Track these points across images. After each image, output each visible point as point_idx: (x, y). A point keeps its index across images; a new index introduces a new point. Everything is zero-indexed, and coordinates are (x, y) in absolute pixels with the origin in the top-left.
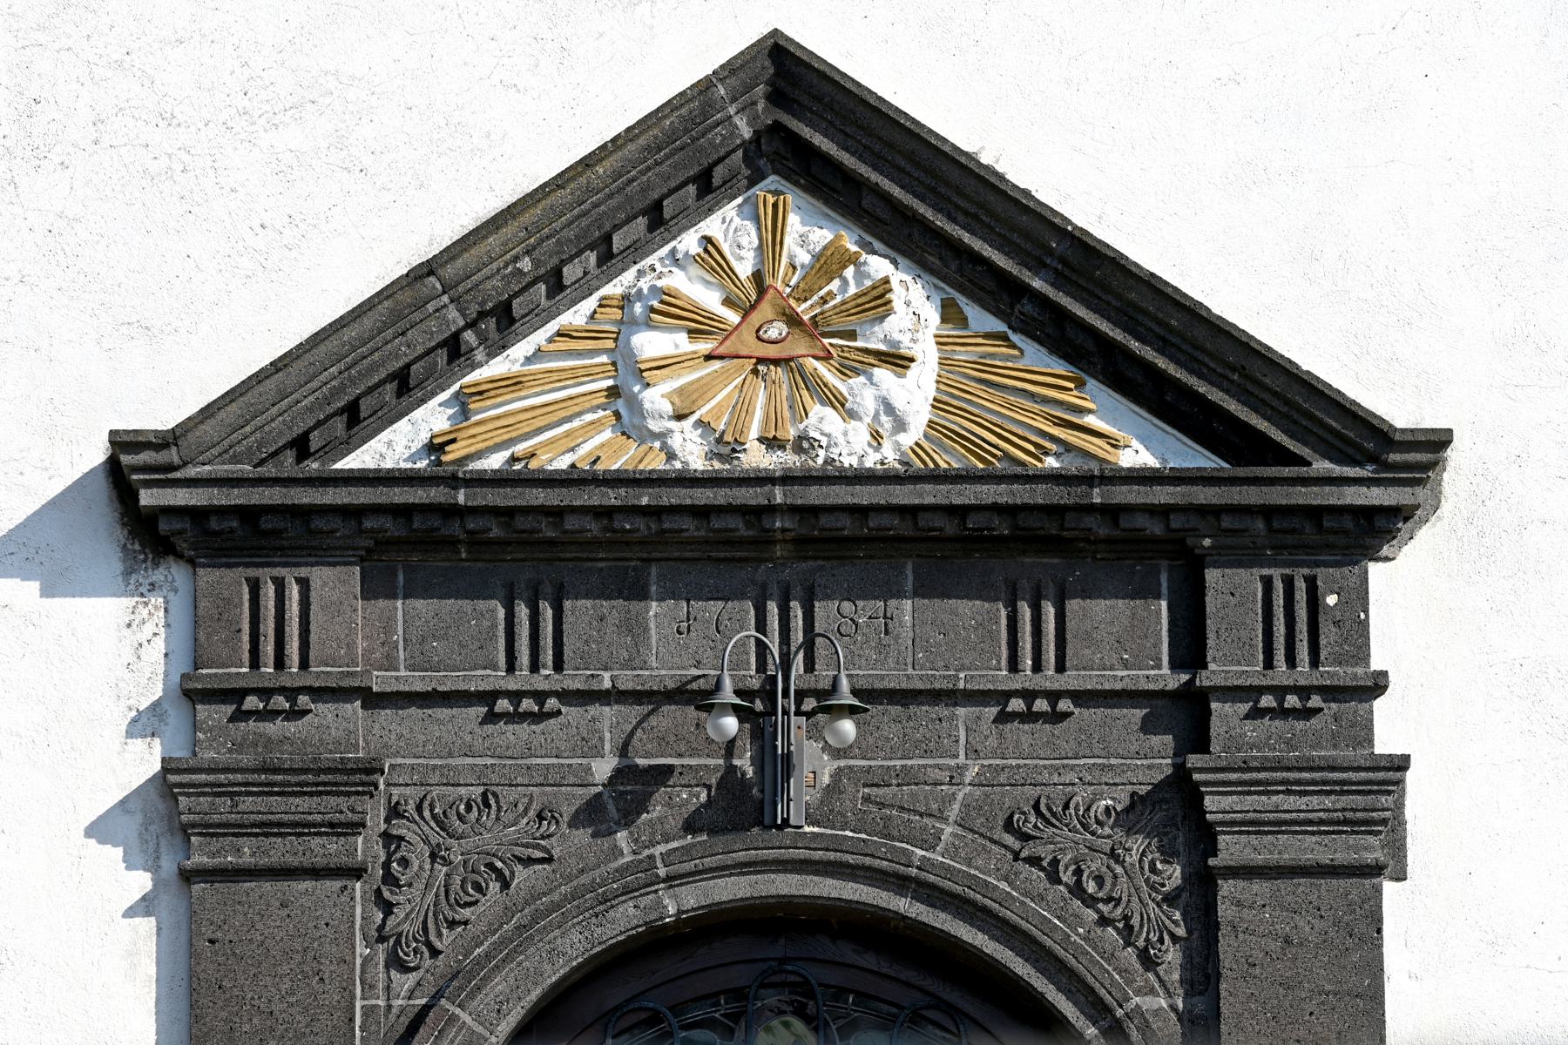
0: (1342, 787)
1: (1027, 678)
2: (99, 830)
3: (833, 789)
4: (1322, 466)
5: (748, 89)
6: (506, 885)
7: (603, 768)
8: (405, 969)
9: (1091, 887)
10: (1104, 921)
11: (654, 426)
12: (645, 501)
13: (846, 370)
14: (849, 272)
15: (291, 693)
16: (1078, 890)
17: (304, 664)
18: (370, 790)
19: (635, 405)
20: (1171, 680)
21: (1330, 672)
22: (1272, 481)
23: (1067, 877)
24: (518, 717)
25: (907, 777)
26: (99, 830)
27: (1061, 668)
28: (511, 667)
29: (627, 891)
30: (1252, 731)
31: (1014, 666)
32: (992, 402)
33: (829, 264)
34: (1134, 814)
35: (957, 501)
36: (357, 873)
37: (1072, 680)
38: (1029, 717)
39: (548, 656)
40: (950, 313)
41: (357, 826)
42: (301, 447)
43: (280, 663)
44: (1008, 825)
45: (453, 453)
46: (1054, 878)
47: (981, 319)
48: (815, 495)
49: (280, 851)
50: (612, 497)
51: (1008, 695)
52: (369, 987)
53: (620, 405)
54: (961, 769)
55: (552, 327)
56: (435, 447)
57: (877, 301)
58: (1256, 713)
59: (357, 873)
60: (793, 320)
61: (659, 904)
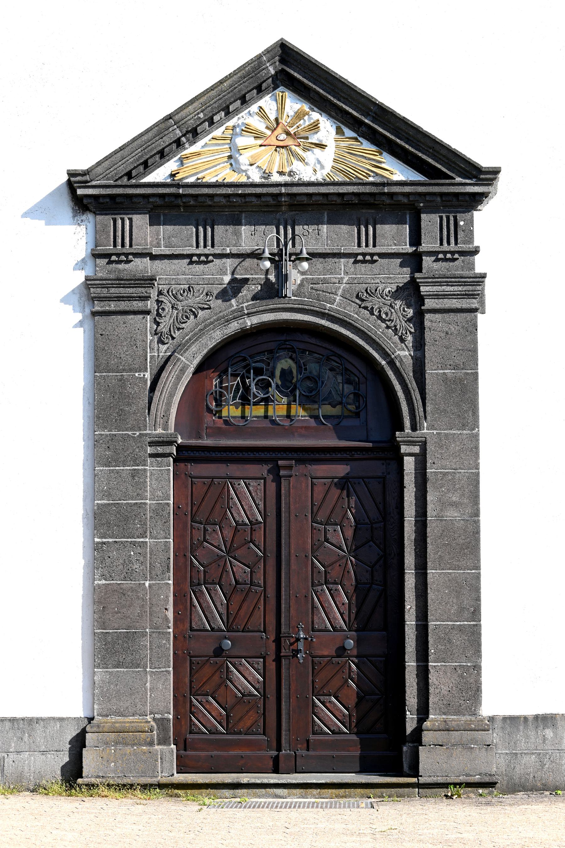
0: (465, 284)
1: (363, 249)
2: (65, 300)
3: (301, 285)
4: (458, 180)
5: (273, 58)
6: (196, 316)
7: (227, 279)
8: (164, 343)
9: (384, 316)
10: (388, 327)
11: (243, 168)
12: (240, 192)
13: (305, 150)
14: (306, 118)
15: (126, 255)
16: (379, 317)
17: (131, 246)
18: (152, 286)
19: (237, 161)
20: (410, 250)
21: (462, 247)
22: (443, 185)
23: (376, 313)
24: (199, 263)
25: (325, 281)
26: (65, 300)
27: (374, 246)
28: (197, 247)
29: (235, 318)
30: (436, 266)
31: (359, 245)
32: (352, 160)
33: (299, 115)
34: (398, 293)
35: (341, 191)
36: (148, 312)
37: (378, 250)
38: (364, 262)
39: (209, 243)
40: (339, 131)
41: (147, 298)
42: (129, 175)
43: (123, 245)
44: (357, 297)
45: (178, 177)
46: (372, 313)
47: (349, 133)
48: (295, 190)
49: (123, 306)
50: (230, 191)
51: (357, 254)
52: (152, 349)
53: (232, 161)
54: (342, 279)
55: (210, 136)
56: (173, 175)
57: (315, 127)
58: (437, 260)
59: (148, 312)
60: (288, 134)
61: (245, 322)
